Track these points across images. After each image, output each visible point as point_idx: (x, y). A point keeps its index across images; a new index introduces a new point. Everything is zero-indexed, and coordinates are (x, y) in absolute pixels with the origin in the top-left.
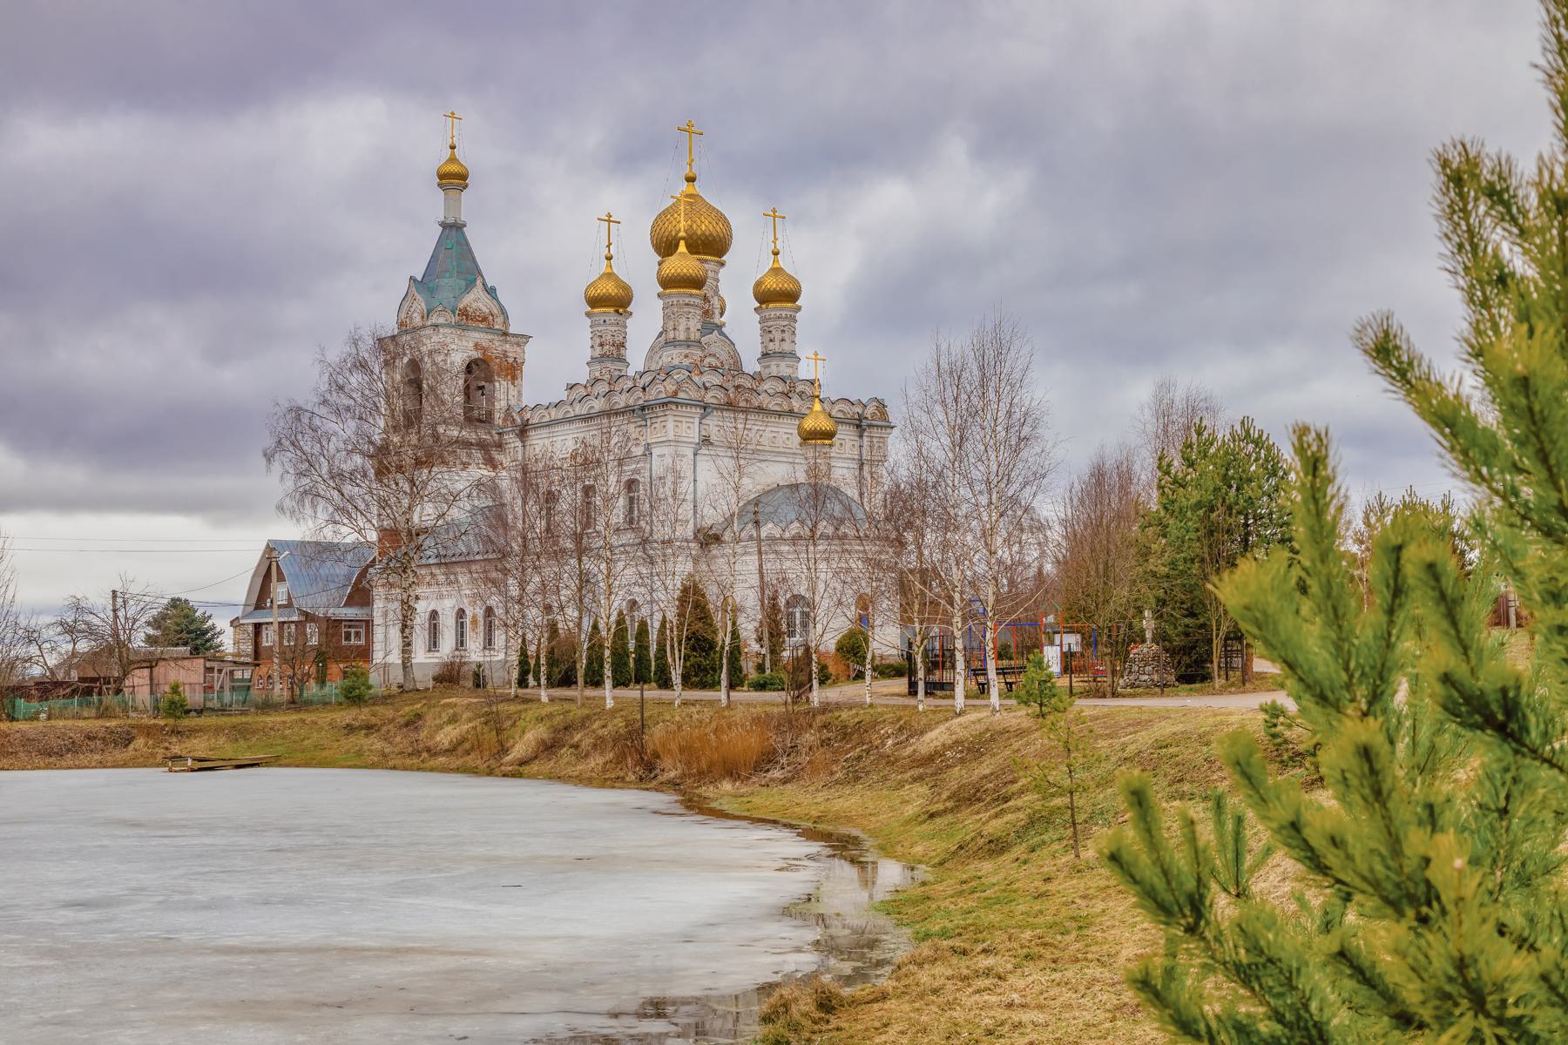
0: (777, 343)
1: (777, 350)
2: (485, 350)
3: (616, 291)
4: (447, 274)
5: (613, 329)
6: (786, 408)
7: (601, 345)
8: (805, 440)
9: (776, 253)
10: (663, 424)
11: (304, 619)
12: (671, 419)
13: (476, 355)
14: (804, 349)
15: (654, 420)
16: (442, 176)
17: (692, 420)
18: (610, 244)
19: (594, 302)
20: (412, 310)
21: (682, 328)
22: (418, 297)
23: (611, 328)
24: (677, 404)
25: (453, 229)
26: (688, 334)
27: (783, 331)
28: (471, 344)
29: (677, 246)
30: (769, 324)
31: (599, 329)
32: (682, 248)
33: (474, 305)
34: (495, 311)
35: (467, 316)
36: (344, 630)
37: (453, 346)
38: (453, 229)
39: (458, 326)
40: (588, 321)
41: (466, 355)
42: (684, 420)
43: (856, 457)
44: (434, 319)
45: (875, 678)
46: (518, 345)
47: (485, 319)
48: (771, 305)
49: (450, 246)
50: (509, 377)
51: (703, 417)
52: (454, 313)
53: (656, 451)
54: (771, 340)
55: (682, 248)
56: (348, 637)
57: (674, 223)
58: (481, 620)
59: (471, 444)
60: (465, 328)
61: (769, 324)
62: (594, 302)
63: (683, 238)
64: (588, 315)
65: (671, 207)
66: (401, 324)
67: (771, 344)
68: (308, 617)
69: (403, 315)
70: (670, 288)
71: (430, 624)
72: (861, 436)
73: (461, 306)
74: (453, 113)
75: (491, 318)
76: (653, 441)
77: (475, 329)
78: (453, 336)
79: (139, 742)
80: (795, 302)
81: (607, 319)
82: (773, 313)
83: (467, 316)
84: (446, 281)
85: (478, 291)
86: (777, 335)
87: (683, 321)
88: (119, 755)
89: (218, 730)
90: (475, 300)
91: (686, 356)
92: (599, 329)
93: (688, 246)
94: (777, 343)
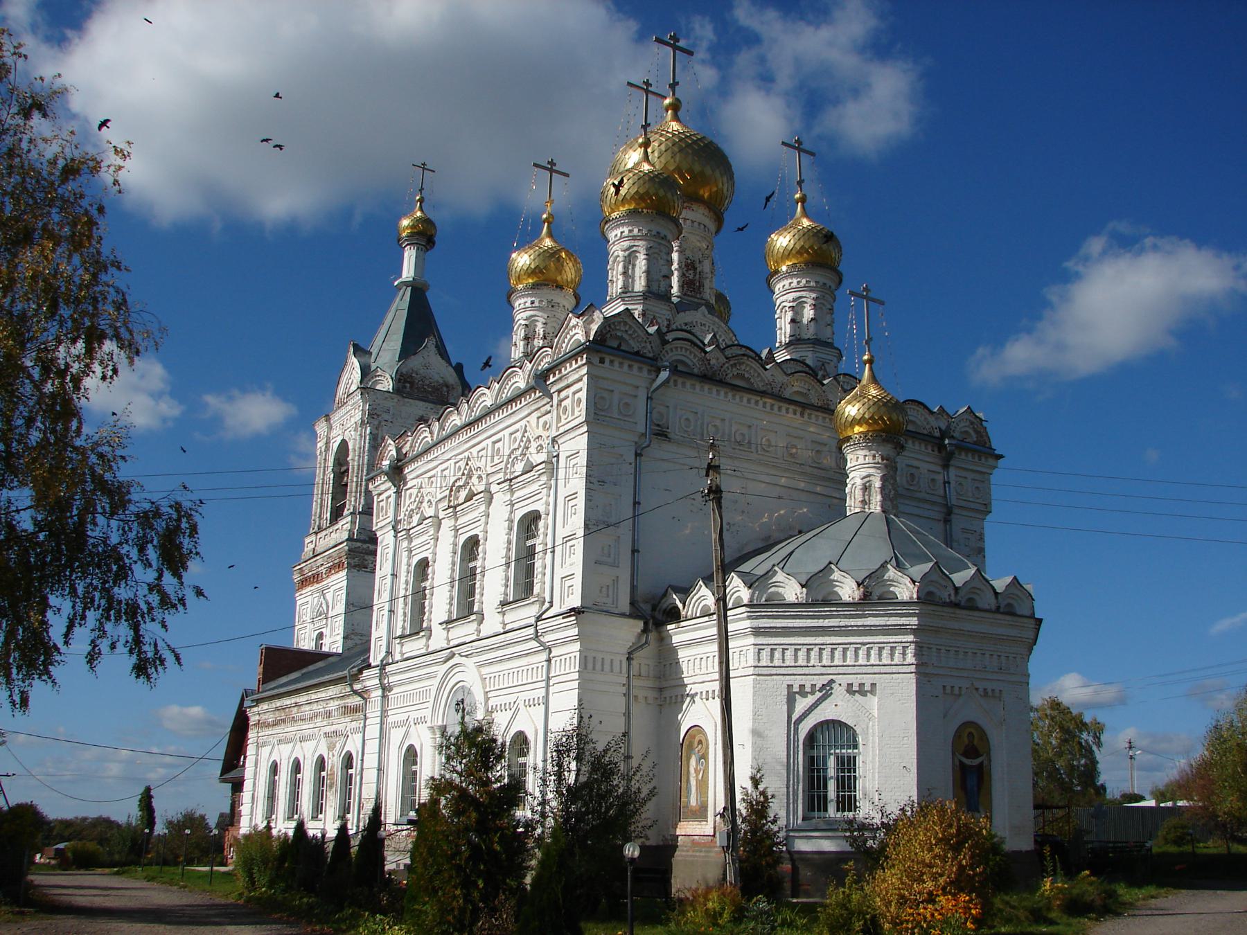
43: (940, 500)
72: (946, 466)
76: (562, 430)
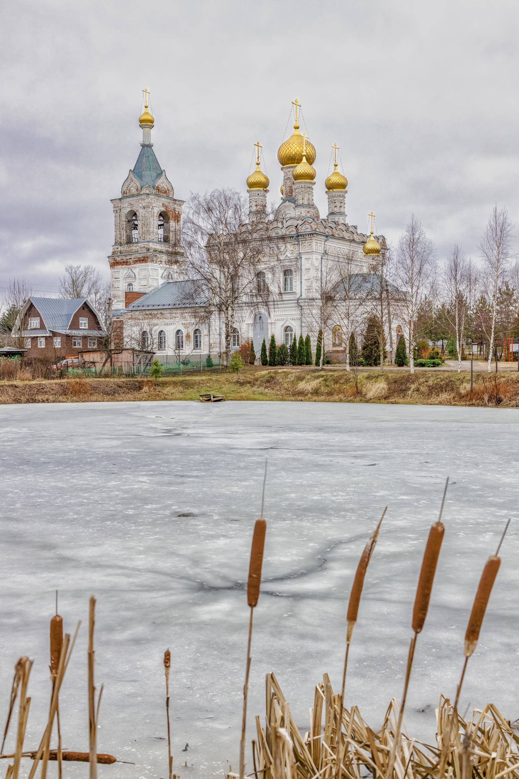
0: (338, 208)
1: (338, 211)
2: (166, 207)
3: (264, 180)
4: (148, 169)
5: (262, 198)
6: (351, 238)
7: (256, 206)
8: (367, 253)
9: (336, 166)
10: (309, 244)
11: (51, 335)
12: (314, 241)
13: (163, 209)
14: (347, 210)
15: (303, 242)
16: (141, 121)
17: (321, 242)
18: (259, 157)
19: (251, 185)
20: (130, 186)
21: (306, 199)
22: (135, 180)
23: (261, 198)
24: (317, 234)
25: (146, 147)
26: (309, 202)
27: (341, 202)
28: (161, 204)
29: (301, 160)
30: (335, 199)
31: (256, 198)
32: (304, 160)
33: (161, 185)
34: (170, 189)
35: (159, 190)
36: (73, 341)
37: (154, 205)
38: (146, 147)
39: (156, 195)
40: (248, 195)
41: (159, 209)
42: (319, 242)
44: (144, 191)
45: (462, 360)
46: (180, 205)
47: (165, 192)
48: (335, 190)
49: (148, 156)
50: (176, 221)
51: (325, 241)
52: (154, 188)
53: (304, 257)
54: (335, 207)
55: (304, 160)
56: (75, 345)
57: (290, 148)
58: (192, 334)
59: (163, 252)
60: (159, 196)
61: (335, 199)
62: (251, 185)
63: (305, 156)
64: (248, 191)
65: (288, 141)
66: (124, 193)
67: (336, 208)
68: (55, 334)
69: (125, 189)
70: (297, 179)
71: (194, 336)
73: (157, 185)
74: (146, 90)
75: (168, 192)
76: (303, 252)
77: (163, 197)
78: (155, 200)
79: (145, 389)
80: (344, 189)
81: (259, 193)
82: (336, 194)
83: (159, 190)
84: (148, 172)
85: (162, 179)
86: (338, 204)
87: (306, 195)
88: (137, 394)
89: (175, 384)
90: (161, 183)
91: (308, 212)
92: (256, 198)
93: (307, 160)
94: (338, 208)
